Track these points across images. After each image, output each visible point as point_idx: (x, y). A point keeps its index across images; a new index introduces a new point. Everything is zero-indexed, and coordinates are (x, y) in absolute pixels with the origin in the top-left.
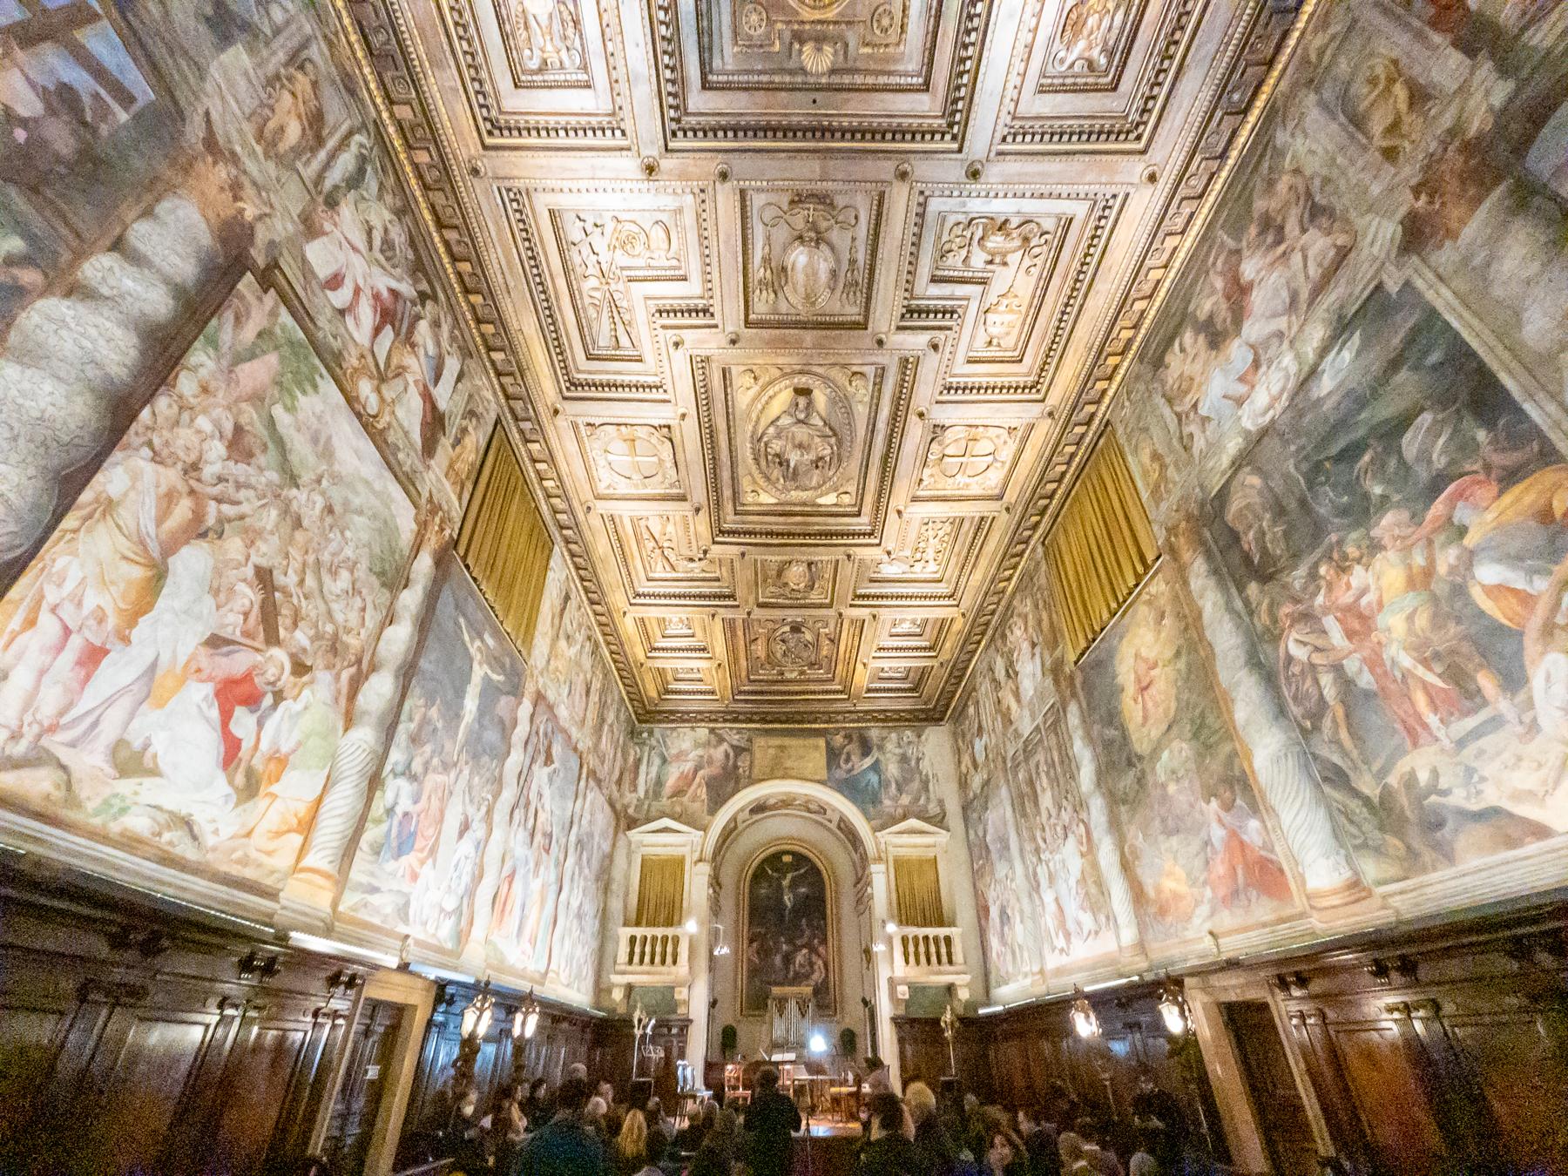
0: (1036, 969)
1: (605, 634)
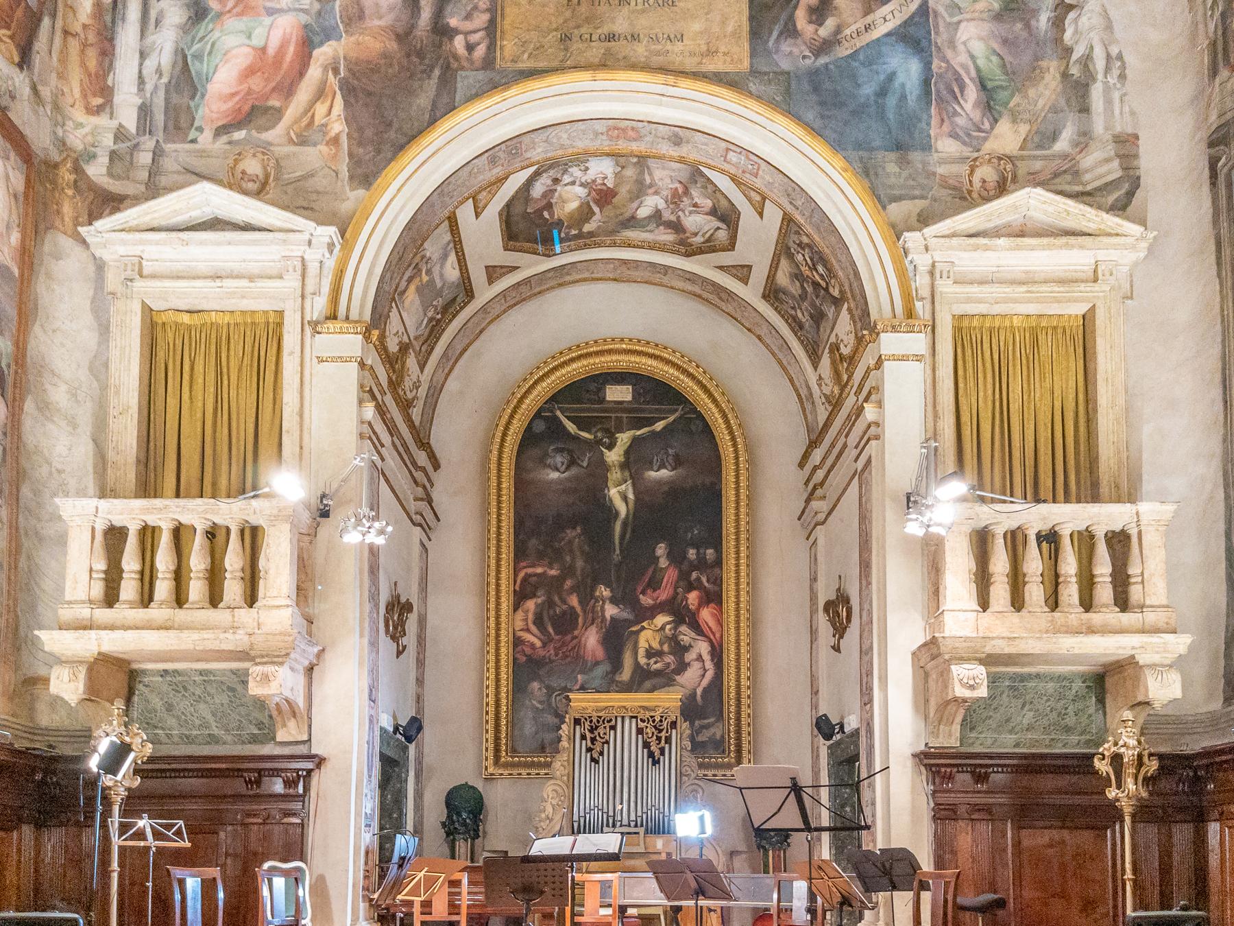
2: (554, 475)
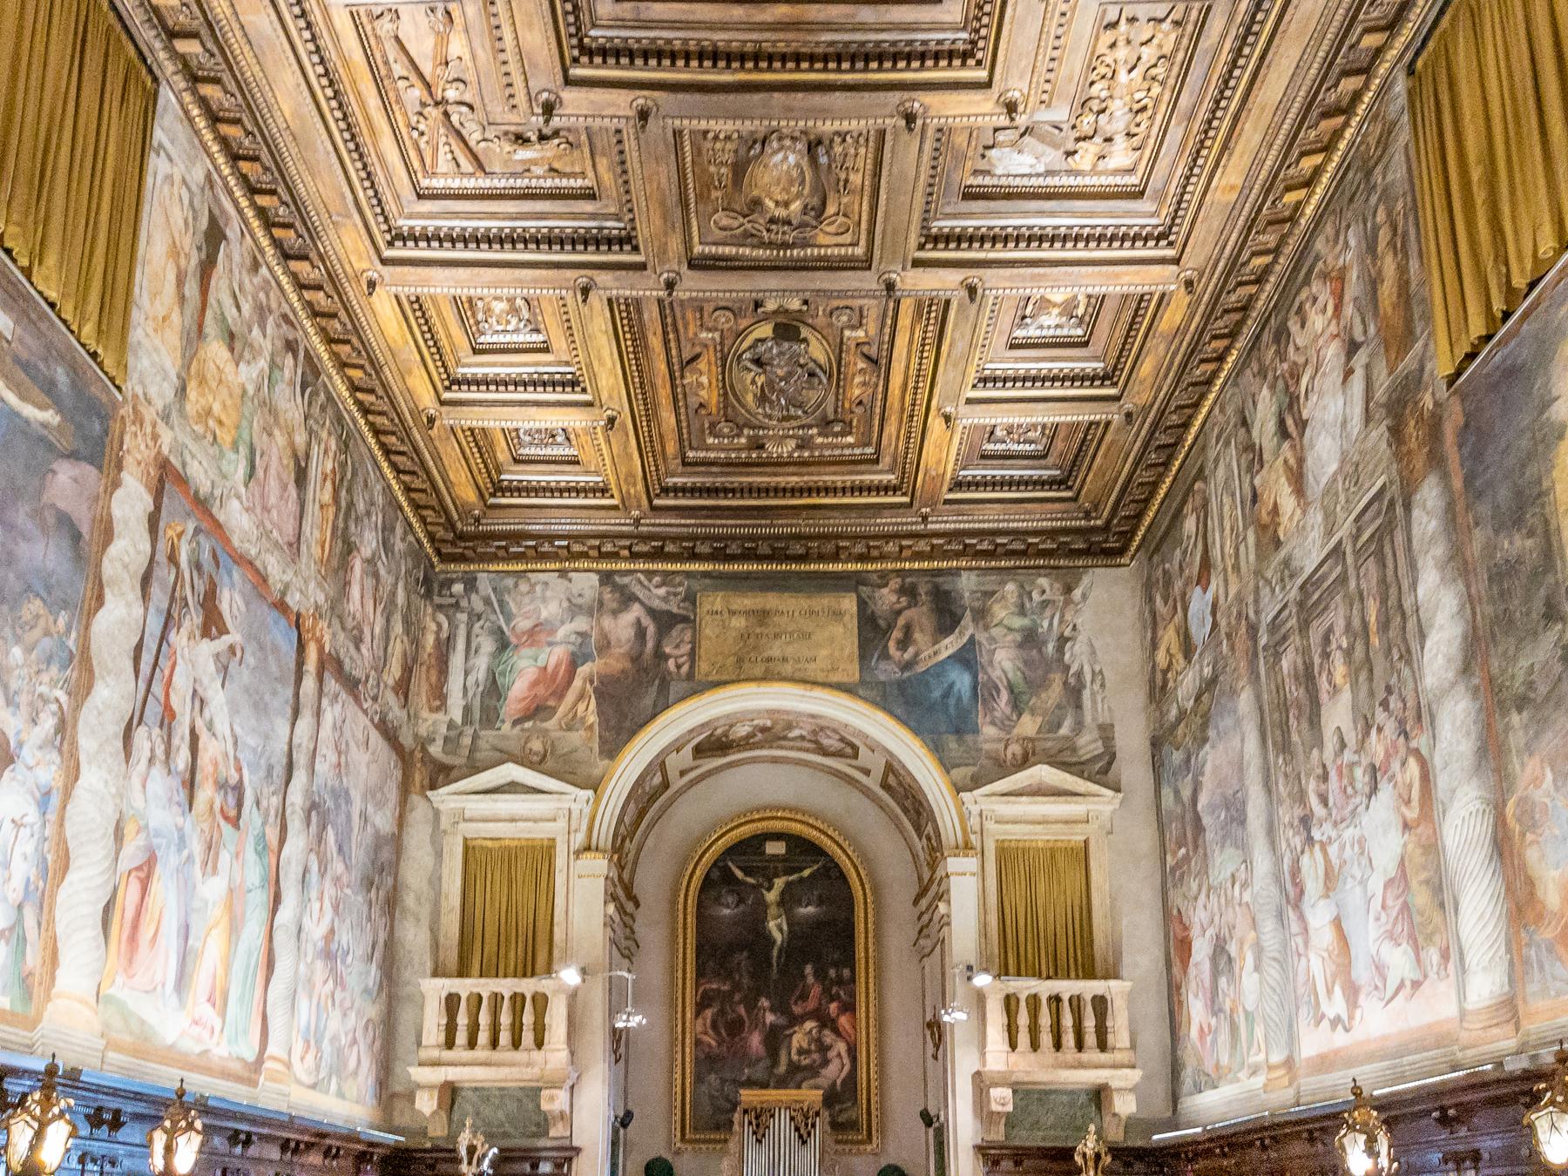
0: (1276, 1058)
1: (330, 341)
2: (727, 912)
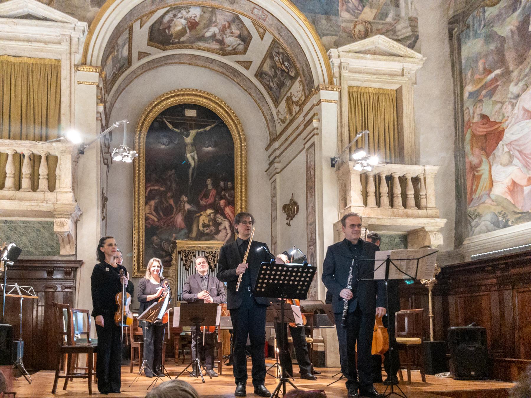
2: (163, 147)
